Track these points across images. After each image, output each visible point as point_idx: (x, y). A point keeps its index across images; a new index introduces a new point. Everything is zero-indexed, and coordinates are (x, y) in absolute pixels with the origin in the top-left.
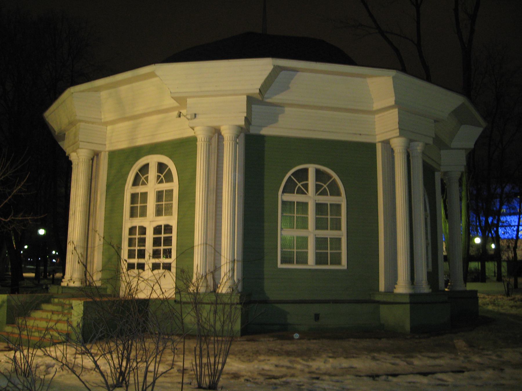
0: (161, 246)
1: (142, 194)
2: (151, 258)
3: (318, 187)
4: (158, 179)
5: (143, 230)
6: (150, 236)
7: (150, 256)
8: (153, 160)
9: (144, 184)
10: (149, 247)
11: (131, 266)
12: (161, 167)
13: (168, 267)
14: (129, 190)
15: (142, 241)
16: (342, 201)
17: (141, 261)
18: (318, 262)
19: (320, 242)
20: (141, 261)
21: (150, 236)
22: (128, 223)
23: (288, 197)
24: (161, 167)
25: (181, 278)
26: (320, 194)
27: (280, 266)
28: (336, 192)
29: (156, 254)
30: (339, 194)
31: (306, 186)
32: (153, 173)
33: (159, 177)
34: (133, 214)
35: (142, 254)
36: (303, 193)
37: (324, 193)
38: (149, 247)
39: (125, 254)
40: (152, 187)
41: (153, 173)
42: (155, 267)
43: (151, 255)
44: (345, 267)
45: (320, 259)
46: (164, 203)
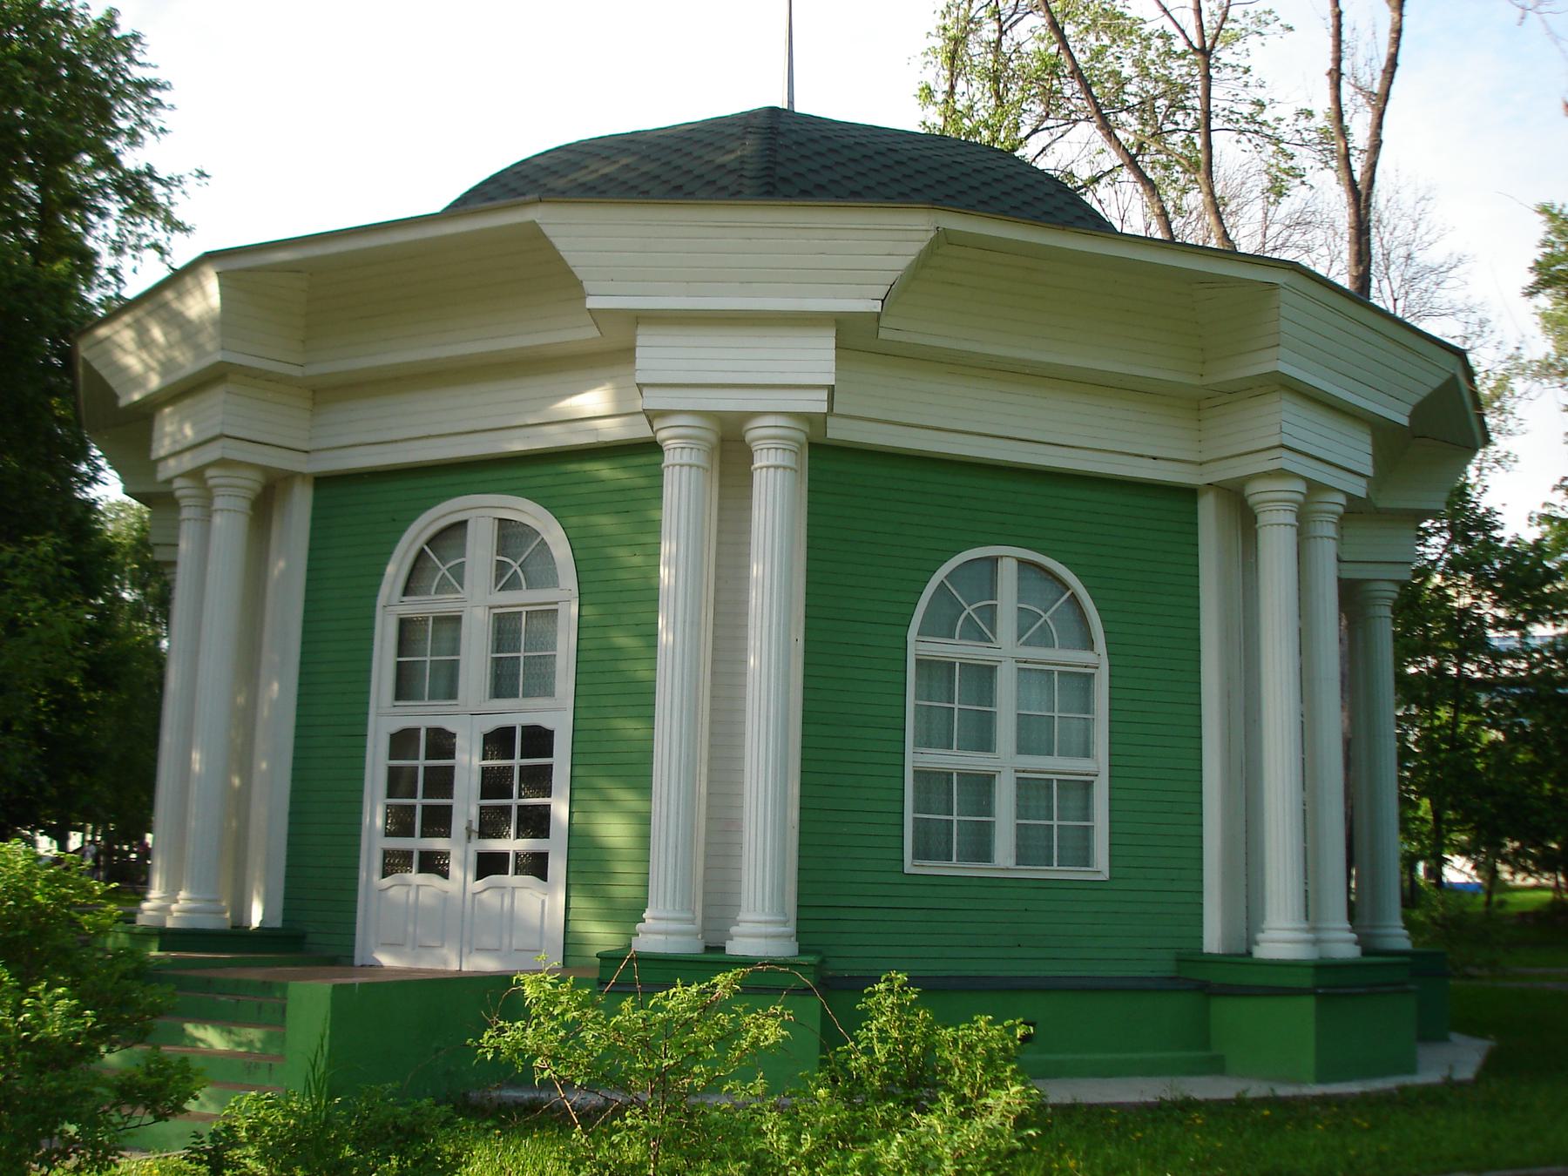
0: (512, 757)
1: (438, 620)
2: (474, 836)
3: (1026, 618)
4: (499, 577)
5: (442, 743)
6: (469, 762)
7: (469, 830)
8: (482, 511)
9: (444, 587)
10: (466, 803)
11: (394, 863)
12: (510, 534)
13: (536, 866)
14: (391, 606)
15: (441, 782)
16: (1098, 659)
17: (438, 844)
18: (1021, 859)
19: (1031, 790)
20: (438, 844)
21: (469, 762)
22: (385, 717)
23: (1008, 574)
24: (510, 534)
25: (1070, 88)
26: (1024, 644)
27: (909, 867)
28: (1089, 644)
29: (491, 824)
30: (1089, 644)
31: (990, 614)
32: (480, 550)
33: (501, 567)
34: (405, 687)
35: (438, 821)
36: (982, 637)
37: (1044, 639)
38: (466, 803)
39: (375, 816)
40: (476, 602)
41: (480, 550)
42: (490, 865)
43: (476, 826)
44: (1105, 876)
45: (1030, 847)
46: (521, 655)
